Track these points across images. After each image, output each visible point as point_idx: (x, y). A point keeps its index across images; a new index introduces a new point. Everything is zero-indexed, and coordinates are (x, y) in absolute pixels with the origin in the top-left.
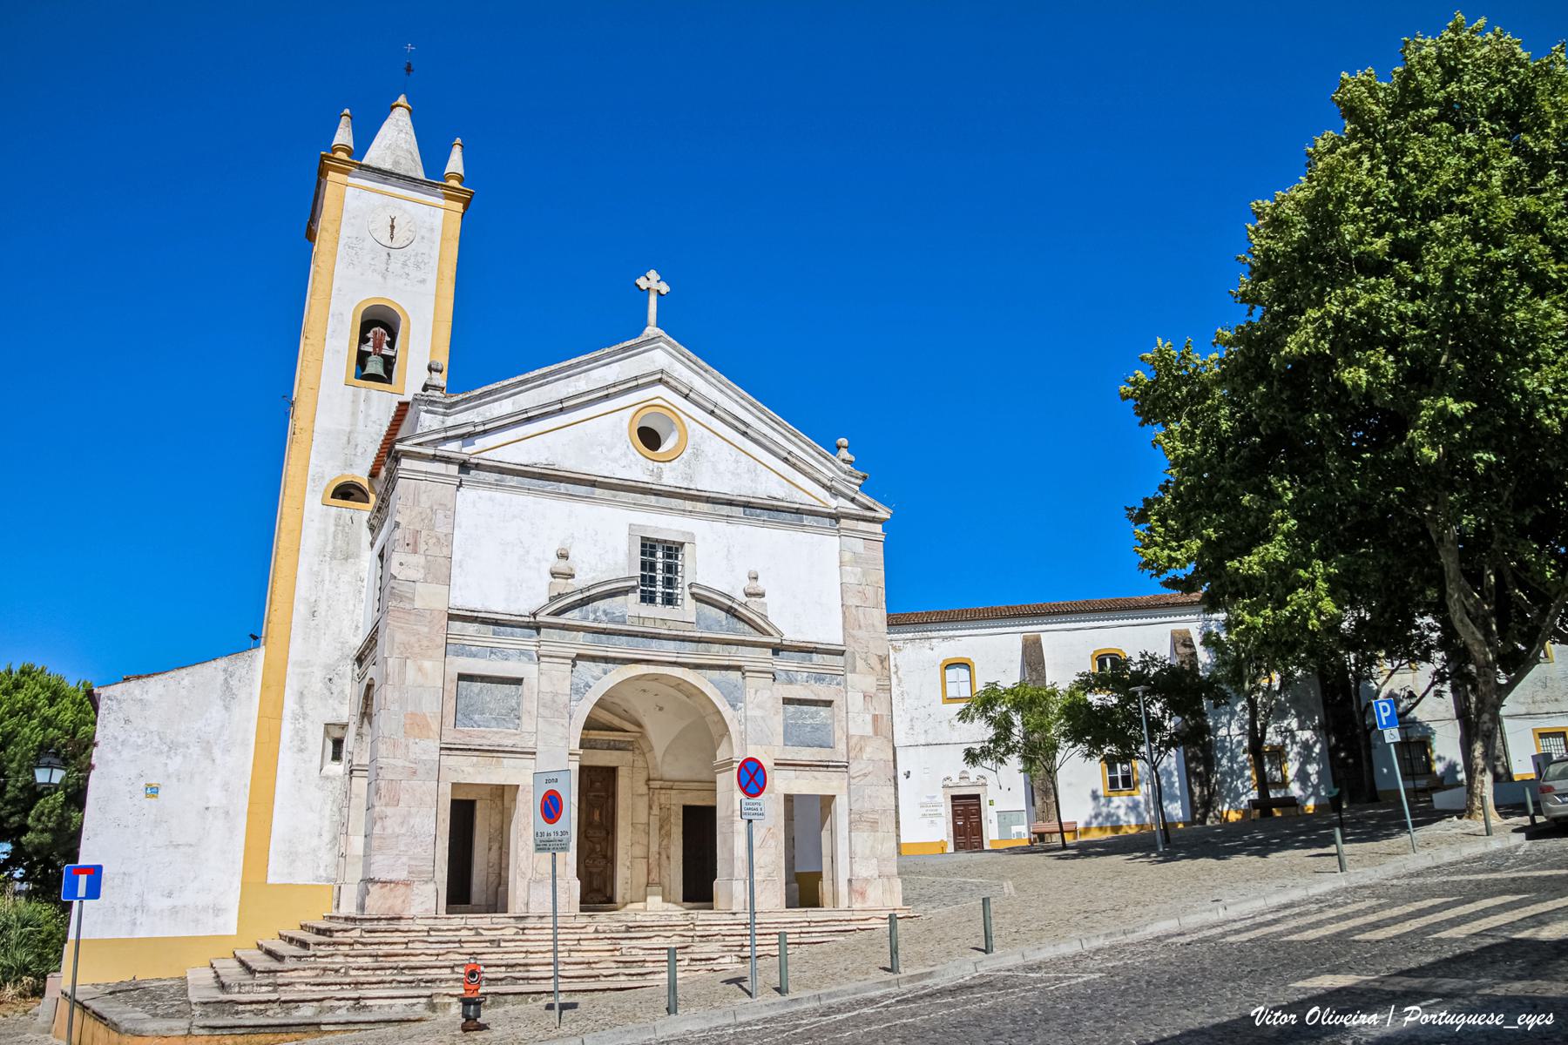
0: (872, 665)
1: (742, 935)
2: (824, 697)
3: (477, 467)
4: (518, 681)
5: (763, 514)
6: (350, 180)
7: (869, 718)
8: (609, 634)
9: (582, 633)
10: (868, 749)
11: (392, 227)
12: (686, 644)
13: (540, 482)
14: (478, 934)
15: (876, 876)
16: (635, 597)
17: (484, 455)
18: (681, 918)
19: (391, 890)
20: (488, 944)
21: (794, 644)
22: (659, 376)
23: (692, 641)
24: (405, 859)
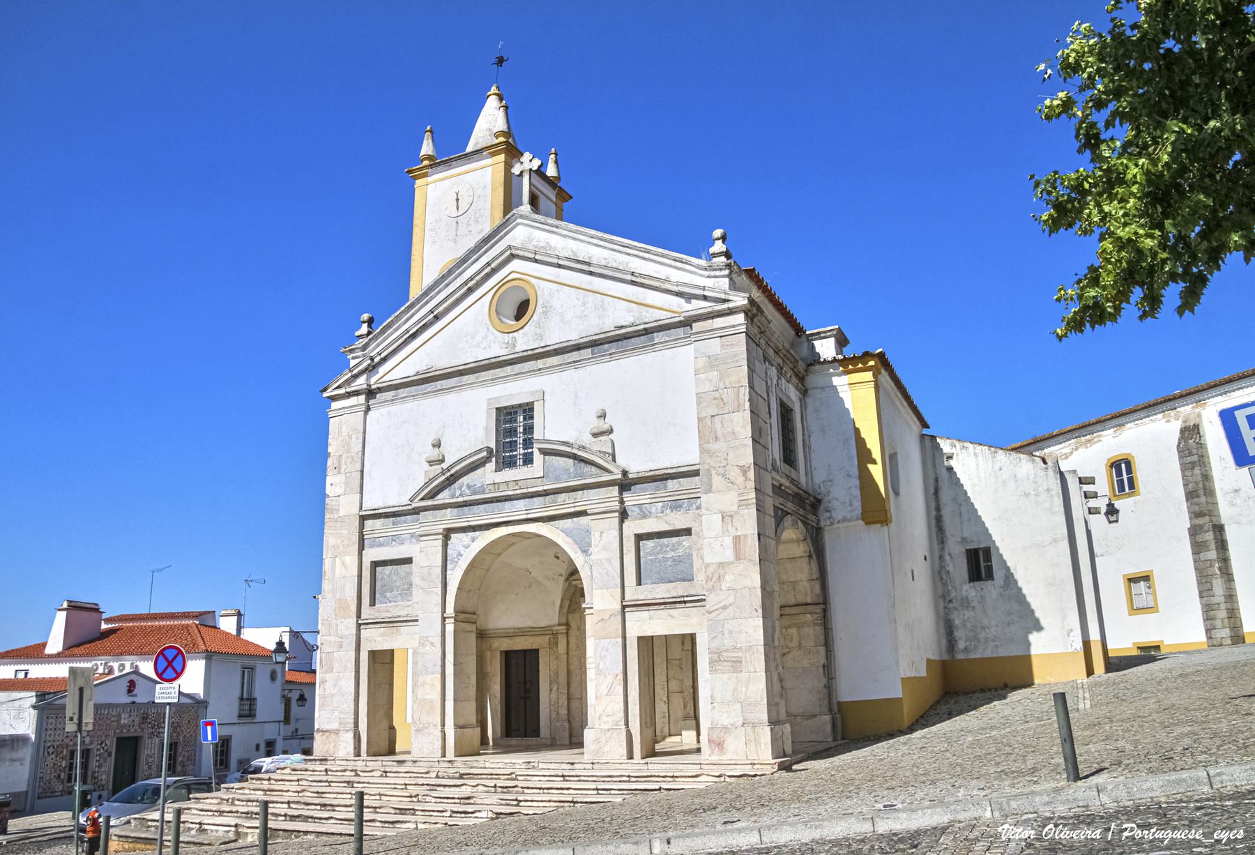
0: (733, 479)
1: (540, 789)
2: (679, 526)
3: (380, 390)
4: (408, 561)
5: (611, 347)
6: (430, 179)
7: (729, 541)
8: (470, 505)
9: (449, 509)
10: (728, 578)
11: (457, 200)
12: (535, 499)
13: (423, 386)
14: (357, 775)
15: (740, 723)
16: (491, 466)
17: (385, 379)
18: (523, 766)
19: (327, 737)
20: (346, 785)
21: (641, 475)
22: (508, 253)
23: (539, 496)
24: (337, 713)
